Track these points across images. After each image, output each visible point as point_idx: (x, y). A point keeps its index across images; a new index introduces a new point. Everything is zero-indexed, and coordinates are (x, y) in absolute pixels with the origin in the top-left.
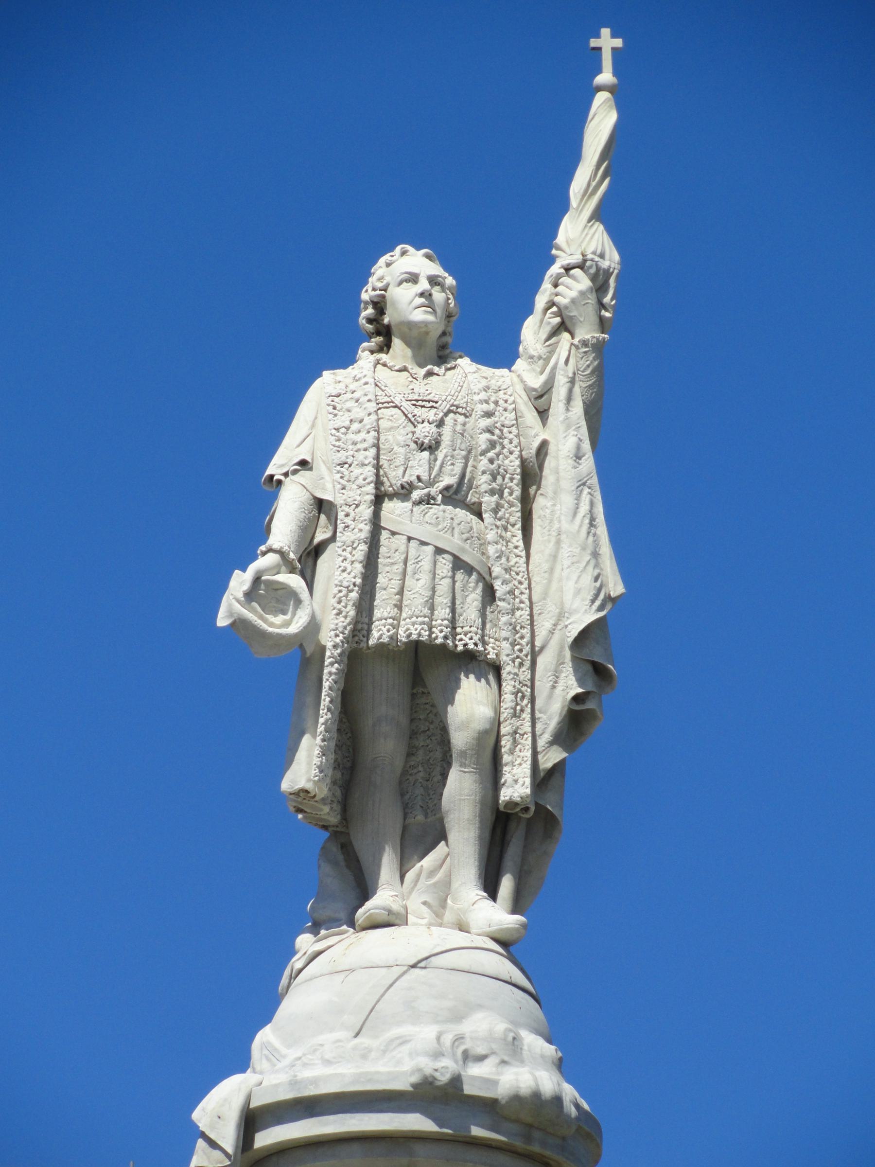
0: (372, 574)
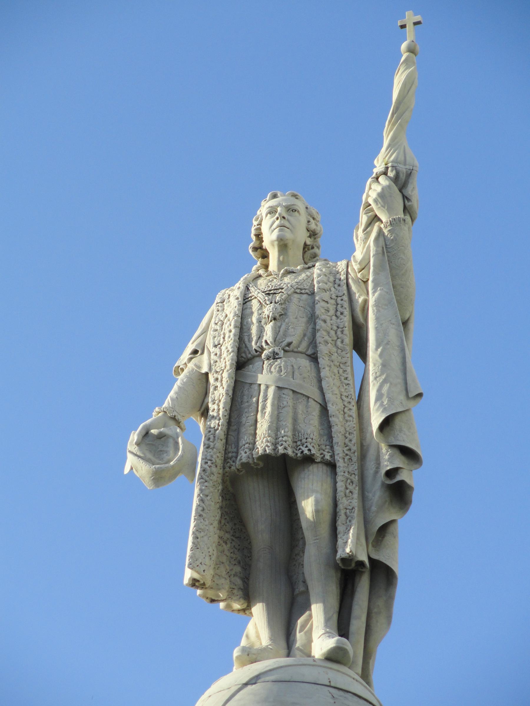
0: (238, 417)
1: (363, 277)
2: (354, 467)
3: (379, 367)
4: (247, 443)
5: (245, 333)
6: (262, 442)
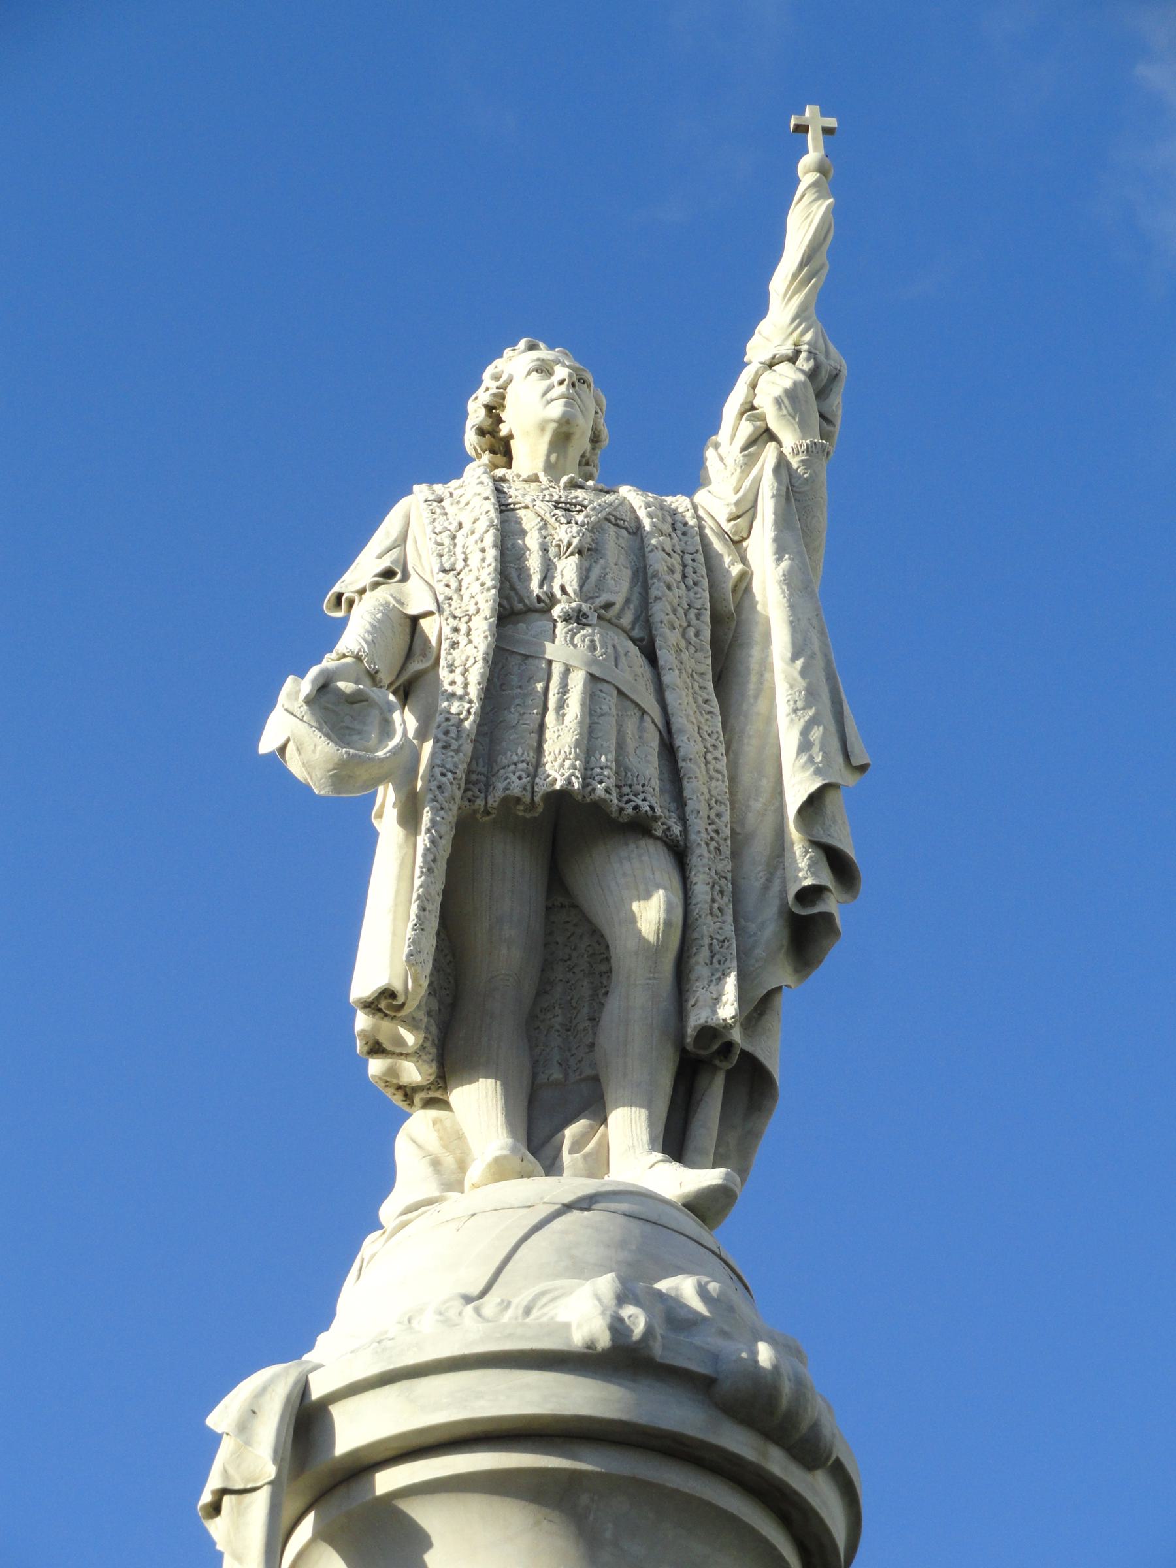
0: (493, 712)
1: (735, 533)
2: (726, 866)
3: (800, 693)
4: (523, 761)
5: (510, 562)
6: (562, 766)
